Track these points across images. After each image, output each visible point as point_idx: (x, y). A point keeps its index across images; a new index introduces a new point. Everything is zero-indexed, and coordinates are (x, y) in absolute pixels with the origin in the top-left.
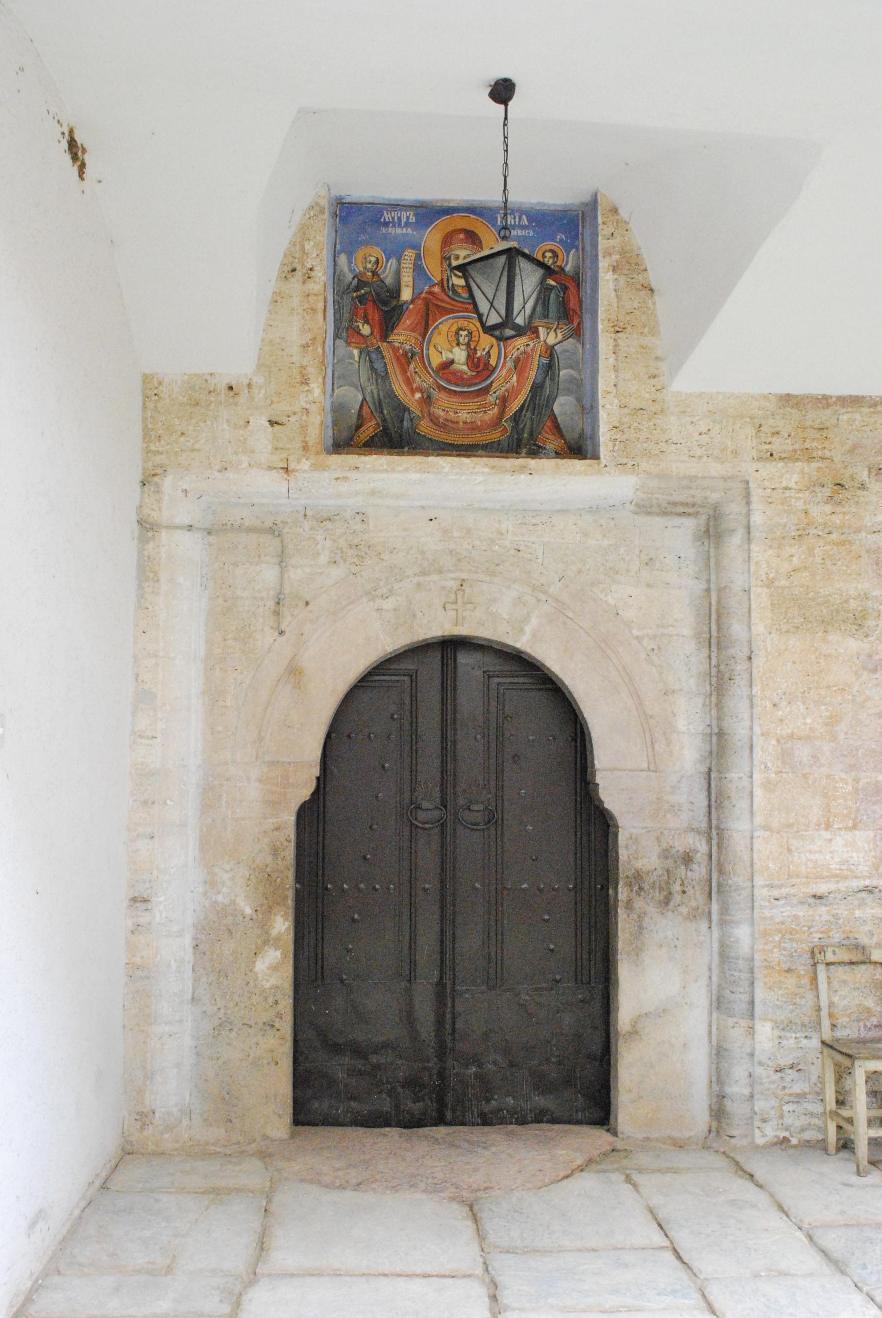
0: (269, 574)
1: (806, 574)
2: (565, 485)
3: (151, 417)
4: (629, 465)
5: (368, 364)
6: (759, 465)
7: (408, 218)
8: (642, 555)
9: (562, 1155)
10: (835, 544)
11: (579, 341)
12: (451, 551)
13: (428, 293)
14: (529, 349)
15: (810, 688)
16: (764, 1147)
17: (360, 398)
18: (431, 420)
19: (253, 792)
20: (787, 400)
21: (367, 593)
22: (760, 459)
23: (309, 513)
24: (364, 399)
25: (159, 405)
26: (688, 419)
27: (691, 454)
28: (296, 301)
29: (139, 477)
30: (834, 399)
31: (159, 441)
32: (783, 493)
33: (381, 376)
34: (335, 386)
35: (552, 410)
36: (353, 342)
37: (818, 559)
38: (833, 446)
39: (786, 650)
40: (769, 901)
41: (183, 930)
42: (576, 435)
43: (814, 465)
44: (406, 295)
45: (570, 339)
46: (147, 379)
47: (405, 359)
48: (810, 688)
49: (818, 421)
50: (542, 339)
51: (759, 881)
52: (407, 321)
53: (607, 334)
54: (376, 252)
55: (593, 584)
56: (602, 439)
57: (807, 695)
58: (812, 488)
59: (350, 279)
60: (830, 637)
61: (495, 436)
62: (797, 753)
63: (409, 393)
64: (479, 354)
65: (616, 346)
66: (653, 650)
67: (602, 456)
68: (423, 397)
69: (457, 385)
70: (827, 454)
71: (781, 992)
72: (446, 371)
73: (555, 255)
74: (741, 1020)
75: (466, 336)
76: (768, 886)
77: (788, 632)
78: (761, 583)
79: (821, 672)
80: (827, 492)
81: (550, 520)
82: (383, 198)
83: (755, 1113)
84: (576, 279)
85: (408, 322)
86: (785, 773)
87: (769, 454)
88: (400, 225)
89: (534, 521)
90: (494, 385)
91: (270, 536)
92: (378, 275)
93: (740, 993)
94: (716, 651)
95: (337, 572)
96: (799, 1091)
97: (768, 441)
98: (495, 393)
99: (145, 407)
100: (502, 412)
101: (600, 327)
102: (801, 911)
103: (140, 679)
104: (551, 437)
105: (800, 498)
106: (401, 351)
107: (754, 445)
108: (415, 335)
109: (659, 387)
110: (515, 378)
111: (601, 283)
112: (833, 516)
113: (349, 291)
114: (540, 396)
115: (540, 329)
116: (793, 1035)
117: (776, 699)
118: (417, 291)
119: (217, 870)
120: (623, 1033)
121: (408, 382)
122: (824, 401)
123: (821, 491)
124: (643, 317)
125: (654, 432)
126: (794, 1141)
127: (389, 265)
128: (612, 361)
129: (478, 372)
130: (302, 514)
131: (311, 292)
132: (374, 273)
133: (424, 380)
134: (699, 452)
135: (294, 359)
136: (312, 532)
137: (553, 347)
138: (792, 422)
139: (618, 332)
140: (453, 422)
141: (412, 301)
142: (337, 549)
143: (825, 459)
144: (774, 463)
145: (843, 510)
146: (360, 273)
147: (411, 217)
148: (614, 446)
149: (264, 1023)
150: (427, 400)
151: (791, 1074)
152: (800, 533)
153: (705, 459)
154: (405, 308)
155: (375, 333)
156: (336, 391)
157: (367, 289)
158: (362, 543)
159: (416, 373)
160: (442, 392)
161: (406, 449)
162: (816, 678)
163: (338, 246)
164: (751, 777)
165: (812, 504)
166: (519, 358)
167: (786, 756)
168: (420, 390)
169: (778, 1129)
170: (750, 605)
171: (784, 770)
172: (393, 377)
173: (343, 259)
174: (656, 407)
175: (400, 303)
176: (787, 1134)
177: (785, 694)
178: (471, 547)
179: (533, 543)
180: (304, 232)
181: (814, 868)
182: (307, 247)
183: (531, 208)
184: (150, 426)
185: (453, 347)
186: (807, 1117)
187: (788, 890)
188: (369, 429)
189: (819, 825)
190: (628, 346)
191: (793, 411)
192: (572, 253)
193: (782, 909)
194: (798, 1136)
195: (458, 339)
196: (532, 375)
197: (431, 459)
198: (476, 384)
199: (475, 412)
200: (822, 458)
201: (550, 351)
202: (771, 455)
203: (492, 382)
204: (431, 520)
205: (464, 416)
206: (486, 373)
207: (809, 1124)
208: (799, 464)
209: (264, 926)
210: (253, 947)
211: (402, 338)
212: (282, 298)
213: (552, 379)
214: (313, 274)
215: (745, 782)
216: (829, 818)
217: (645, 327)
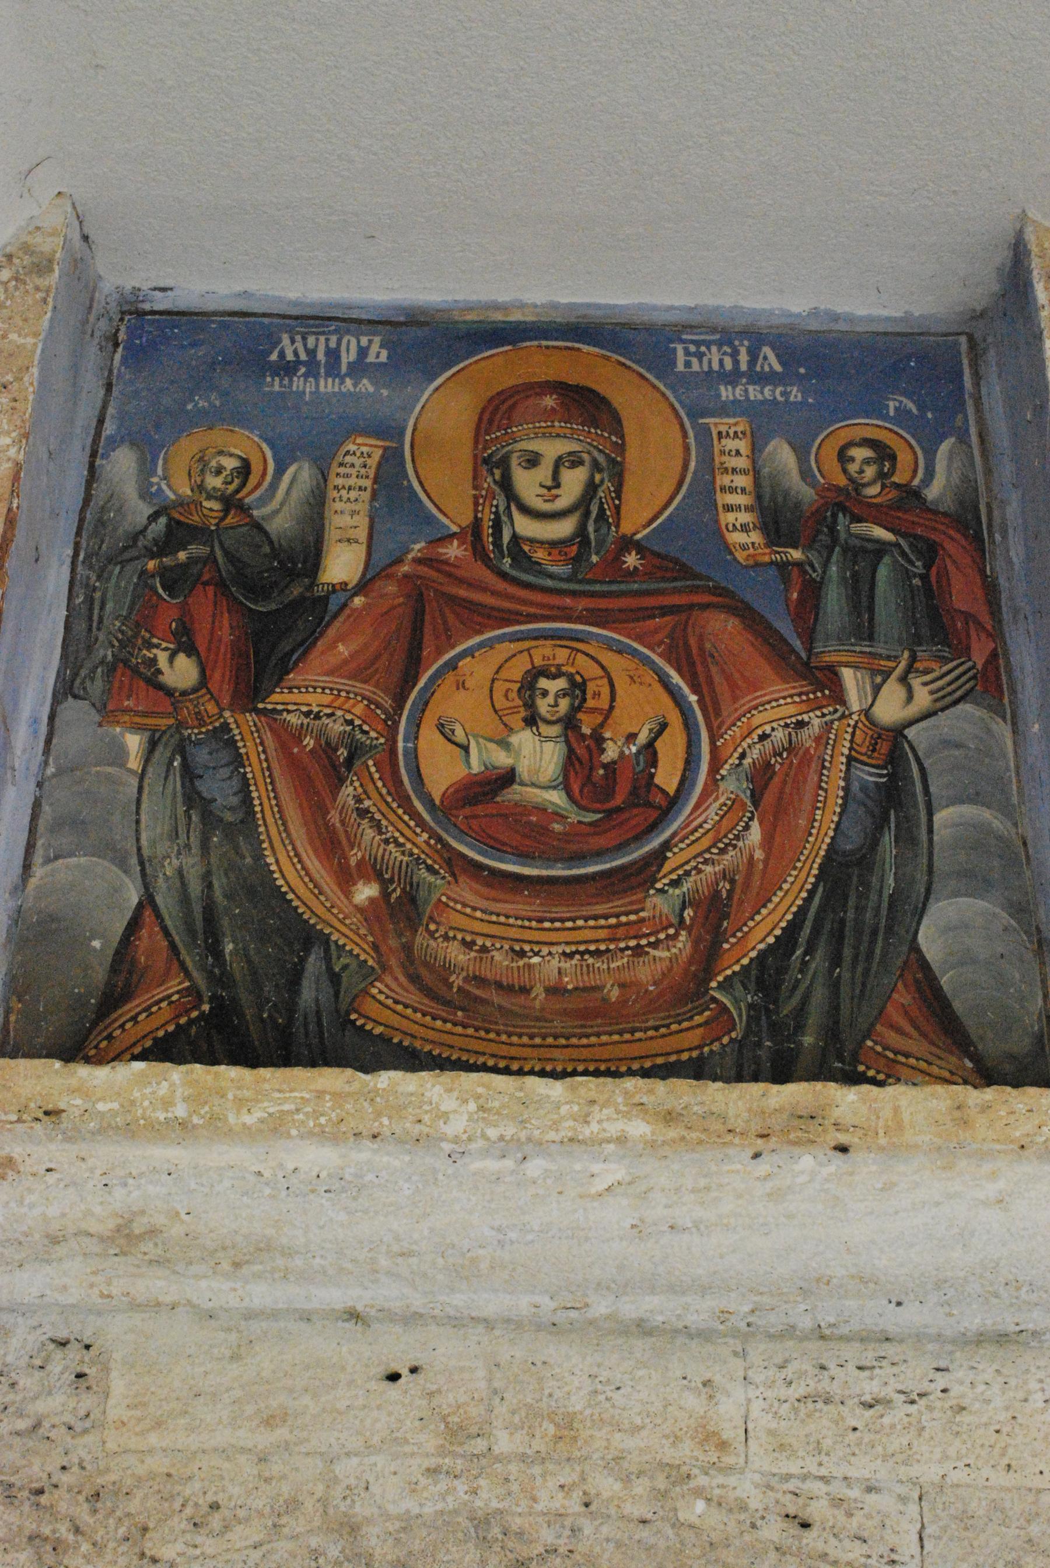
5: (176, 782)
7: (363, 352)
13: (417, 561)
14: (806, 737)
17: (133, 897)
18: (414, 979)
24: (148, 901)
34: (38, 858)
36: (126, 710)
50: (855, 707)
59: (142, 519)
64: (611, 753)
68: (385, 894)
69: (524, 856)
72: (480, 810)
81: (942, 1380)
89: (870, 1388)
92: (243, 509)
104: (915, 1045)
106: (309, 742)
108: (367, 689)
110: (755, 834)
113: (133, 553)
115: (848, 675)
118: (381, 558)
127: (287, 478)
129: (610, 813)
137: (898, 732)
140: (508, 989)
146: (181, 503)
147: (375, 348)
154: (333, 607)
155: (213, 685)
156: (39, 870)
157: (197, 549)
163: (110, 428)
166: (768, 765)
168: (374, 870)
172: (268, 826)
175: (319, 592)
192: (945, 447)
195: (530, 705)
198: (599, 854)
199: (597, 953)
203: (666, 846)
204: (394, 1377)
211: (315, 700)
213: (907, 838)
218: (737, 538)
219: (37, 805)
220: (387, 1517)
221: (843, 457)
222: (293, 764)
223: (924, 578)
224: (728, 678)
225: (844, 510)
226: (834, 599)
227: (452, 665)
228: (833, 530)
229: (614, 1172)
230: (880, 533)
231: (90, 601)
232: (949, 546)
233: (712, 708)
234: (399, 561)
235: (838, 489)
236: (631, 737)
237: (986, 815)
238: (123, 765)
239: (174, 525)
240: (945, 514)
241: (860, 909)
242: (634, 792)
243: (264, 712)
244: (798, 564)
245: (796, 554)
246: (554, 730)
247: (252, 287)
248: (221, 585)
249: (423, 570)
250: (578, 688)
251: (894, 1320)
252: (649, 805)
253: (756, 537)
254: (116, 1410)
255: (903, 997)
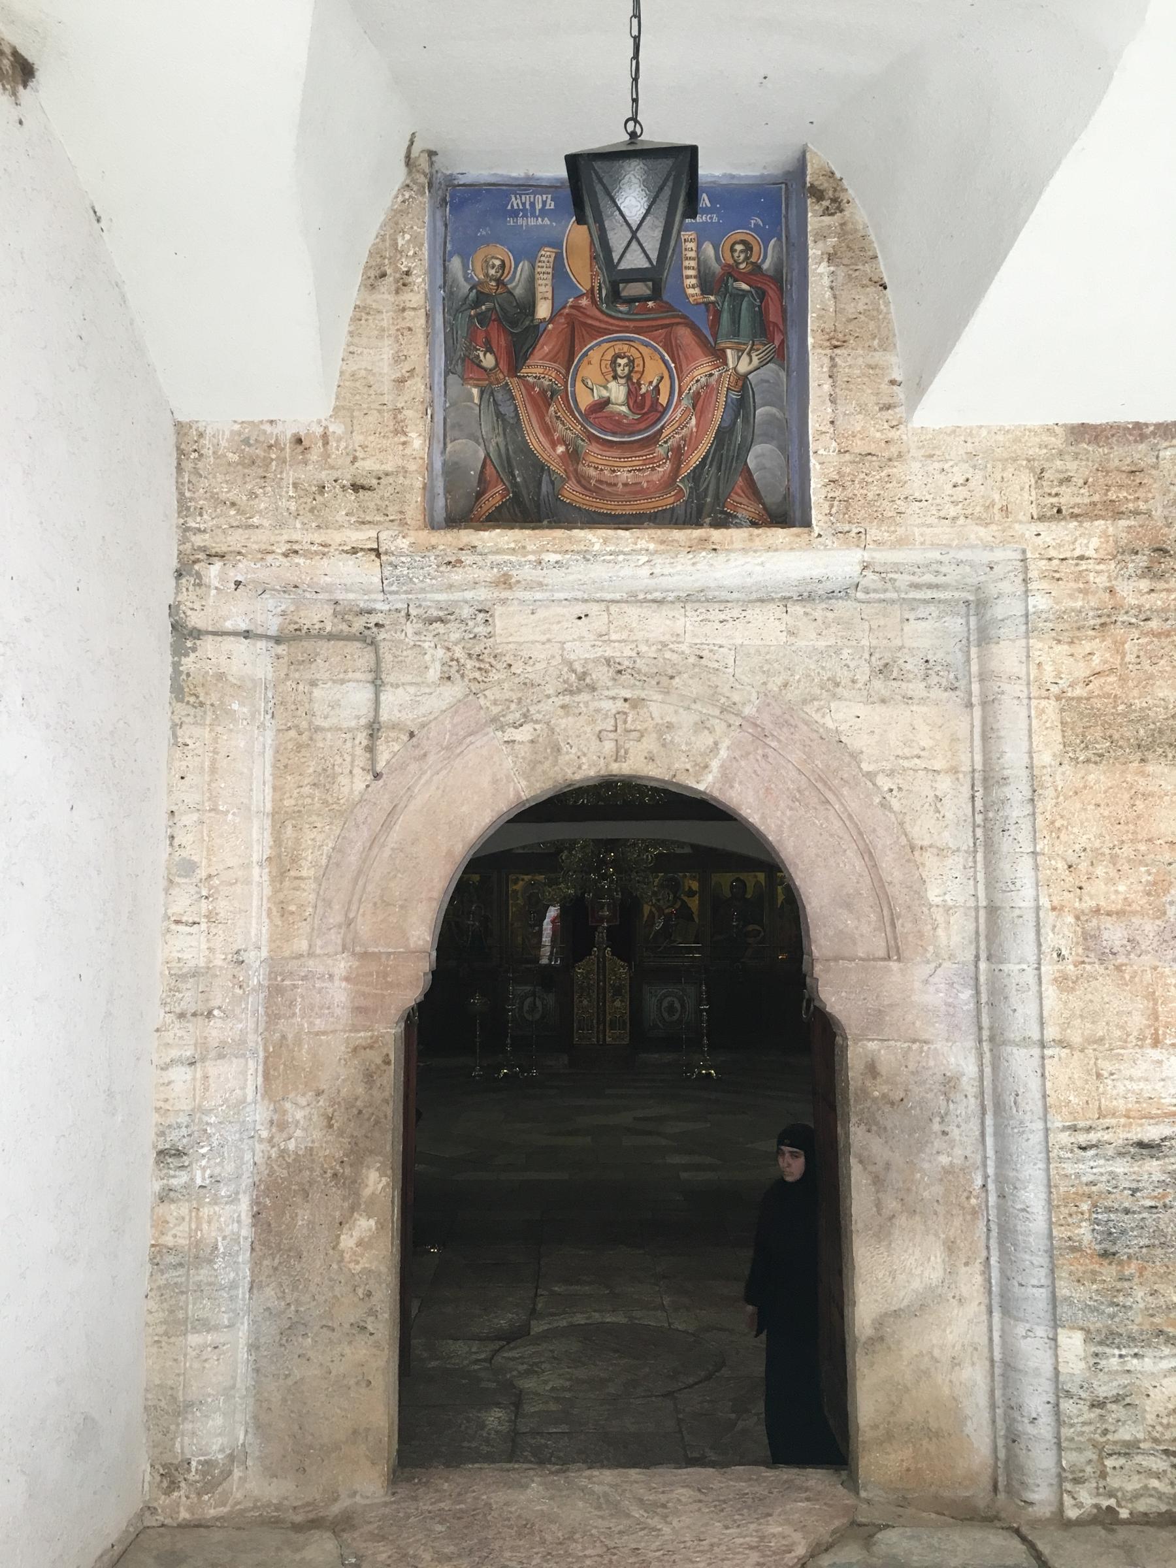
0: (358, 697)
1: (1112, 679)
2: (762, 564)
3: (189, 482)
4: (853, 534)
5: (492, 407)
6: (1041, 527)
7: (544, 203)
8: (873, 658)
9: (774, 1535)
10: (1158, 635)
11: (782, 366)
12: (608, 661)
13: (571, 307)
14: (713, 380)
15: (1123, 842)
16: (1079, 1523)
17: (482, 455)
18: (579, 482)
19: (339, 994)
20: (1082, 433)
21: (494, 720)
22: (1042, 518)
23: (413, 612)
24: (488, 455)
25: (200, 465)
26: (937, 466)
27: (942, 514)
28: (386, 319)
29: (174, 564)
30: (1151, 428)
31: (201, 515)
32: (1077, 565)
33: (510, 425)
34: (448, 440)
35: (746, 463)
36: (471, 378)
37: (1130, 658)
38: (1150, 495)
39: (1085, 787)
40: (1072, 1151)
41: (237, 1193)
42: (778, 498)
43: (1123, 523)
44: (543, 310)
45: (770, 365)
46: (181, 428)
47: (544, 399)
48: (1123, 842)
49: (1129, 460)
50: (731, 366)
51: (1057, 1122)
52: (545, 347)
53: (820, 351)
54: (500, 253)
55: (804, 702)
56: (813, 499)
57: (1119, 852)
58: (1119, 557)
59: (467, 290)
60: (1150, 768)
61: (668, 501)
62: (1105, 935)
63: (547, 445)
64: (643, 390)
65: (834, 366)
66: (891, 790)
67: (814, 522)
68: (567, 450)
69: (614, 434)
70: (1142, 506)
71: (1095, 1287)
72: (599, 415)
73: (748, 247)
74: (1035, 1327)
75: (626, 365)
76: (1069, 1128)
77: (1088, 761)
78: (1045, 693)
79: (1138, 817)
80: (1142, 560)
81: (744, 614)
82: (511, 177)
83: (1064, 1470)
84: (777, 279)
85: (546, 349)
86: (1090, 963)
87: (1055, 510)
88: (533, 215)
89: (722, 616)
90: (665, 433)
91: (358, 645)
92: (505, 285)
93: (1033, 1286)
94: (981, 790)
95: (453, 692)
96: (1127, 1437)
97: (1053, 493)
98: (666, 442)
99: (179, 468)
100: (676, 470)
101: (810, 341)
102: (1120, 1167)
103: (176, 842)
104: (744, 500)
105: (1102, 571)
106: (537, 389)
107: (1033, 498)
108: (555, 365)
109: (894, 423)
110: (693, 421)
111: (812, 279)
112: (1153, 595)
113: (464, 307)
114: (729, 445)
115: (729, 352)
116: (1117, 1352)
117: (1072, 858)
118: (558, 307)
119: (288, 1105)
120: (863, 1339)
121: (548, 431)
122: (1138, 431)
123: (1133, 561)
124: (872, 325)
125: (888, 485)
126: (1124, 1514)
127: (519, 269)
128: (827, 387)
129: (644, 414)
130: (403, 613)
131: (408, 305)
132: (499, 282)
133: (569, 428)
134: (952, 511)
135: (386, 399)
136: (417, 638)
137: (745, 377)
138: (1090, 464)
139: (836, 347)
140: (610, 485)
141: (551, 320)
142: (452, 660)
143: (1139, 514)
144: (1063, 523)
145: (1167, 586)
146: (480, 283)
147: (549, 201)
148: (831, 506)
149: (352, 1325)
150: (574, 456)
151: (1117, 1410)
152: (1103, 620)
153: (961, 521)
154: (541, 329)
155: (501, 366)
156: (449, 446)
157: (489, 305)
158: (486, 651)
159: (558, 418)
160: (594, 444)
161: (545, 522)
162: (1132, 827)
163: (449, 247)
164: (1038, 969)
165: (1120, 579)
166: (699, 393)
167: (1089, 939)
168: (563, 441)
169: (1098, 1495)
170: (1030, 725)
171: (1087, 960)
172: (525, 425)
173: (456, 263)
174: (894, 450)
175: (536, 322)
176: (1112, 1502)
177: (1085, 850)
178: (634, 654)
179: (721, 647)
180: (396, 220)
181: (1137, 1102)
182: (400, 242)
183: (714, 182)
184: (188, 494)
185: (608, 382)
186: (1142, 1476)
187: (1099, 1135)
188: (495, 497)
189: (1144, 1039)
190: (850, 366)
191: (1090, 449)
192: (773, 242)
193: (1092, 1164)
194: (1130, 1505)
195: (615, 371)
196: (717, 416)
197: (576, 532)
198: (640, 432)
199: (639, 470)
200: (1136, 513)
201: (743, 380)
202: (1059, 511)
203: (663, 427)
204: (580, 618)
205: (624, 476)
206: (653, 416)
207: (1146, 1487)
208: (1100, 523)
209: (350, 1185)
210: (337, 1214)
211: (538, 371)
212: (368, 314)
213: (746, 421)
214: (410, 279)
215: (1030, 977)
216: (1156, 1030)
217: (874, 338)
218: (690, 291)
219: (445, 419)
220: (579, 659)
221: (732, 250)
222: (532, 399)
223: (760, 307)
224: (685, 355)
225: (732, 276)
226: (725, 317)
227: (586, 354)
228: (726, 285)
229: (644, 559)
230: (745, 286)
231: (452, 329)
232: (771, 293)
233: (679, 369)
234: (564, 307)
235: (729, 266)
236: (651, 383)
237: (774, 410)
238: (472, 401)
239: (479, 293)
240: (770, 277)
241: (728, 450)
242: (652, 406)
243: (519, 377)
244: (713, 303)
245: (712, 298)
246: (623, 381)
247: (500, 172)
248: (498, 320)
249: (574, 312)
250: (631, 362)
251: (730, 597)
252: (656, 411)
253: (697, 291)
254: (498, 631)
255: (740, 481)
